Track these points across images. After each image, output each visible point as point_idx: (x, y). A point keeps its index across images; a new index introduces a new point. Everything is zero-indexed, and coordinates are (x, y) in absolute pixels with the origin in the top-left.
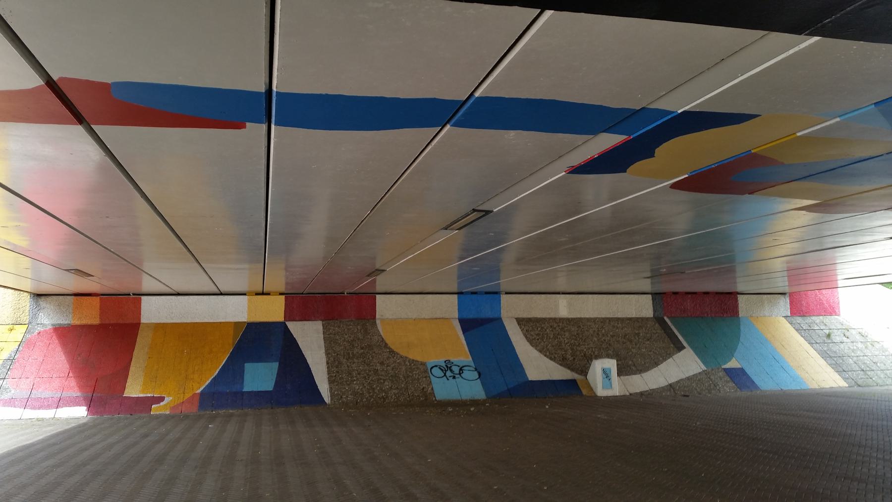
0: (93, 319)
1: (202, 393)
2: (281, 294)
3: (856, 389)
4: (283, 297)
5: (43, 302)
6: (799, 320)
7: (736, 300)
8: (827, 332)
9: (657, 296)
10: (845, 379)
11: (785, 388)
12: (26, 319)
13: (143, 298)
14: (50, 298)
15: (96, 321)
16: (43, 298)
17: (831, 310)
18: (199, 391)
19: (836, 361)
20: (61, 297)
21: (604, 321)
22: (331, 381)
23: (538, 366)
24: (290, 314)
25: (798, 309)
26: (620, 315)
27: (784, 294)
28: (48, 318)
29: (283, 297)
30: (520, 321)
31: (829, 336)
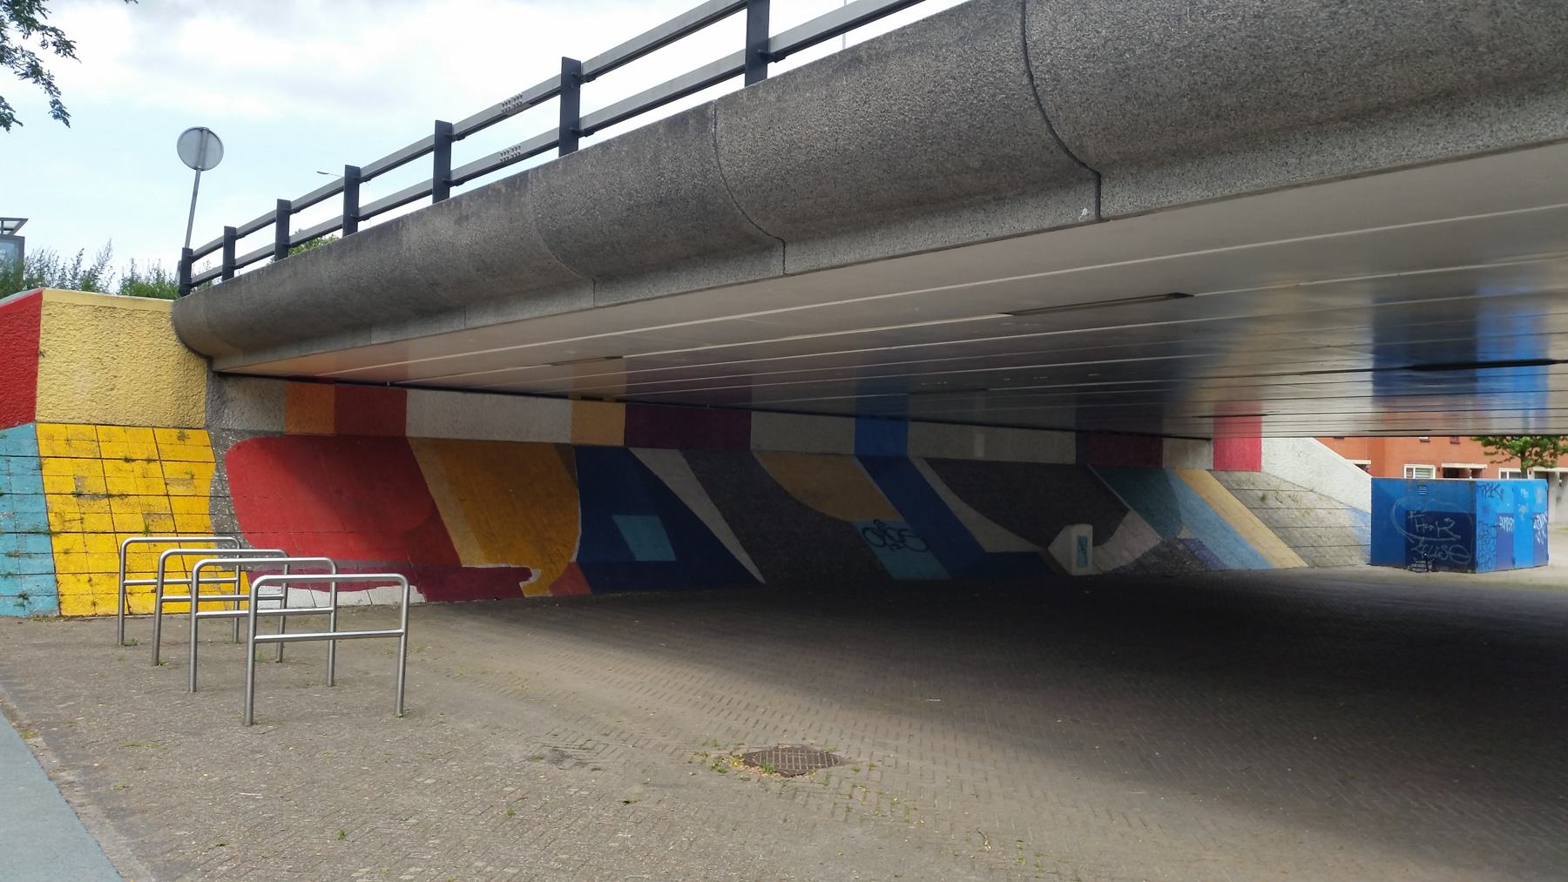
0: (322, 424)
1: (580, 562)
2: (618, 400)
3: (1316, 570)
4: (622, 406)
5: (231, 390)
6: (1224, 475)
7: (1161, 446)
8: (1260, 494)
9: (1082, 435)
10: (1303, 557)
11: (1209, 544)
12: (200, 417)
13: (411, 393)
14: (245, 382)
15: (326, 428)
16: (231, 381)
17: (1254, 463)
18: (574, 559)
19: (1282, 531)
20: (264, 382)
21: (873, 41)
22: (748, 549)
23: (993, 537)
24: (632, 435)
25: (1221, 465)
26: (1041, 460)
27: (1208, 439)
28: (244, 417)
29: (622, 406)
30: (935, 463)
31: (1263, 499)
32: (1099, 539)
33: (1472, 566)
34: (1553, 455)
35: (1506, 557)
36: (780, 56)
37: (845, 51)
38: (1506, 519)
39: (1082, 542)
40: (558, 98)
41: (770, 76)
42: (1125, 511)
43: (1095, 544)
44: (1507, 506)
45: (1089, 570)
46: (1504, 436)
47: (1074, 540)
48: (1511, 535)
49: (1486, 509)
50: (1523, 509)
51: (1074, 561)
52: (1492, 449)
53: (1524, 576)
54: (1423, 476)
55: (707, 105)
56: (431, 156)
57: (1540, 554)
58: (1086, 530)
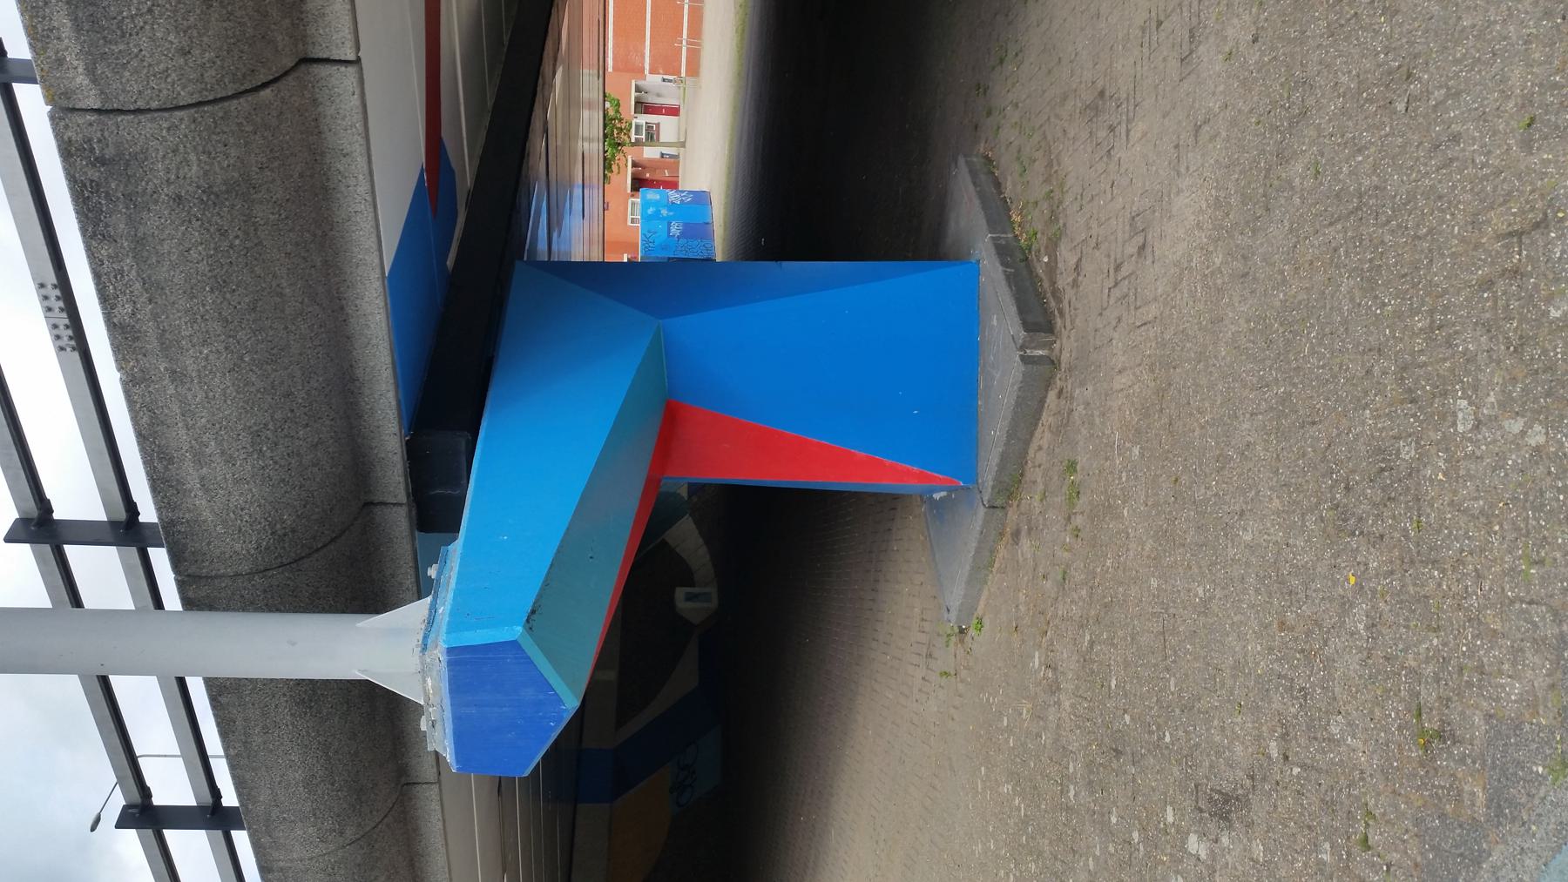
23: (685, 678)
32: (687, 578)
33: (708, 225)
34: (621, 120)
35: (698, 230)
36: (131, 508)
37: (227, 756)
38: (673, 230)
39: (690, 597)
40: (167, 833)
41: (236, 804)
42: (664, 543)
43: (692, 585)
44: (661, 226)
45: (712, 590)
46: (605, 159)
47: (689, 605)
48: (686, 225)
49: (664, 247)
50: (664, 212)
51: (705, 605)
52: (614, 168)
53: (719, 215)
54: (638, 209)
55: (72, 179)
56: (170, 835)
57: (701, 198)
58: (680, 593)
